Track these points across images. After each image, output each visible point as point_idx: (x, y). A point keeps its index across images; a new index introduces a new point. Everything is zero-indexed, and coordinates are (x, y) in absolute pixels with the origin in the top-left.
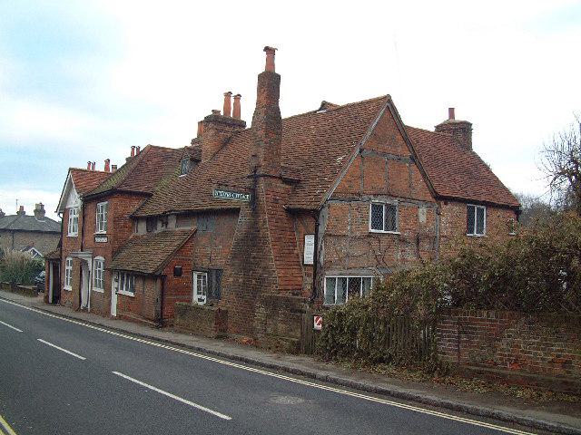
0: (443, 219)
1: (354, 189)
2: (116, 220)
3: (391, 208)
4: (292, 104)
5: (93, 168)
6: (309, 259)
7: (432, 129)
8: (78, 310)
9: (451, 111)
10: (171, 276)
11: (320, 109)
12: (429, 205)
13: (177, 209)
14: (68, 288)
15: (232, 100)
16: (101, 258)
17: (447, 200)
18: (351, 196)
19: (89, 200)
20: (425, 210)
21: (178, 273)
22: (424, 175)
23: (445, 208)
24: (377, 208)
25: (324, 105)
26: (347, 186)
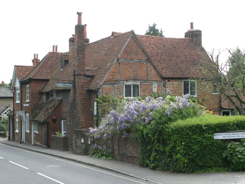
0: (167, 89)
1: (115, 79)
2: (32, 95)
3: (135, 87)
4: (94, 35)
5: (56, 50)
6: (95, 113)
7: (183, 36)
8: (21, 143)
9: (192, 24)
10: (51, 122)
11: (111, 36)
12: (159, 82)
13: (55, 89)
14: (17, 131)
15: (36, 56)
16: (28, 114)
17: (169, 79)
18: (114, 82)
19: (23, 84)
20: (156, 86)
21: (54, 121)
22: (155, 68)
23: (169, 84)
24: (128, 87)
25: (113, 33)
26: (111, 77)
